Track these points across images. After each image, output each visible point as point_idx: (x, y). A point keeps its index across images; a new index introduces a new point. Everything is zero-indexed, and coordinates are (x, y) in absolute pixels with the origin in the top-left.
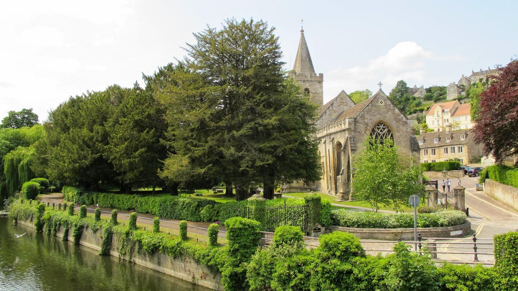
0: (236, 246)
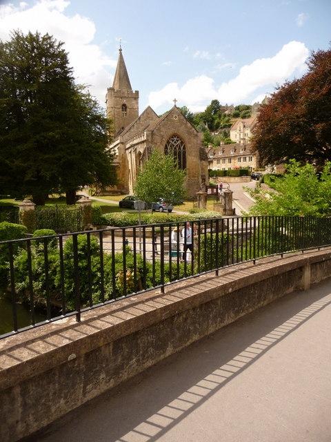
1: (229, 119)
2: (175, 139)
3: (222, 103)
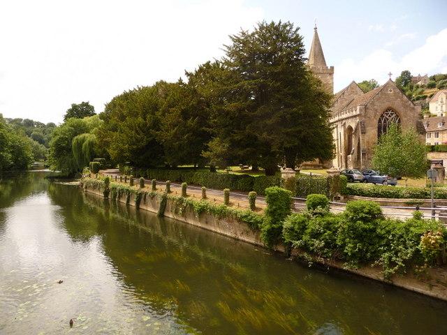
0: (274, 207)
1: (423, 91)
2: (390, 113)
3: (414, 74)
